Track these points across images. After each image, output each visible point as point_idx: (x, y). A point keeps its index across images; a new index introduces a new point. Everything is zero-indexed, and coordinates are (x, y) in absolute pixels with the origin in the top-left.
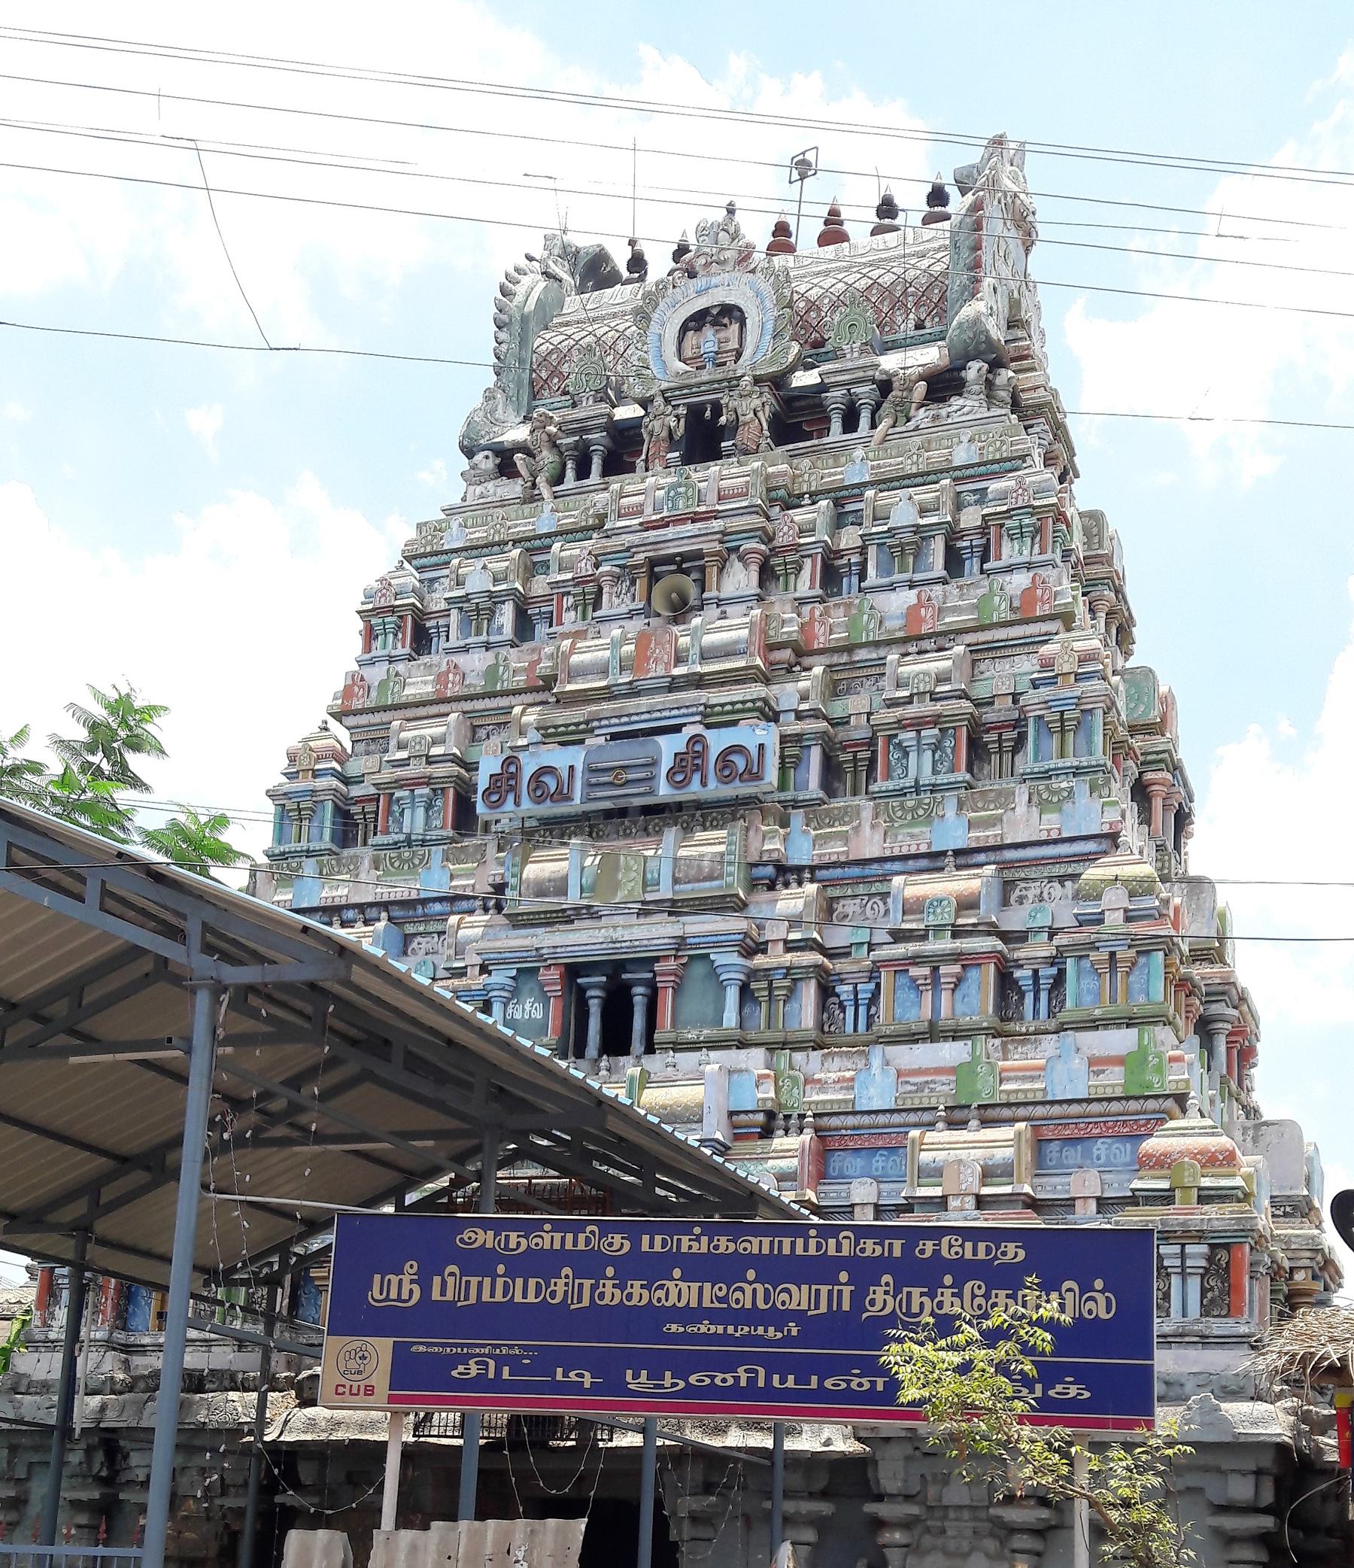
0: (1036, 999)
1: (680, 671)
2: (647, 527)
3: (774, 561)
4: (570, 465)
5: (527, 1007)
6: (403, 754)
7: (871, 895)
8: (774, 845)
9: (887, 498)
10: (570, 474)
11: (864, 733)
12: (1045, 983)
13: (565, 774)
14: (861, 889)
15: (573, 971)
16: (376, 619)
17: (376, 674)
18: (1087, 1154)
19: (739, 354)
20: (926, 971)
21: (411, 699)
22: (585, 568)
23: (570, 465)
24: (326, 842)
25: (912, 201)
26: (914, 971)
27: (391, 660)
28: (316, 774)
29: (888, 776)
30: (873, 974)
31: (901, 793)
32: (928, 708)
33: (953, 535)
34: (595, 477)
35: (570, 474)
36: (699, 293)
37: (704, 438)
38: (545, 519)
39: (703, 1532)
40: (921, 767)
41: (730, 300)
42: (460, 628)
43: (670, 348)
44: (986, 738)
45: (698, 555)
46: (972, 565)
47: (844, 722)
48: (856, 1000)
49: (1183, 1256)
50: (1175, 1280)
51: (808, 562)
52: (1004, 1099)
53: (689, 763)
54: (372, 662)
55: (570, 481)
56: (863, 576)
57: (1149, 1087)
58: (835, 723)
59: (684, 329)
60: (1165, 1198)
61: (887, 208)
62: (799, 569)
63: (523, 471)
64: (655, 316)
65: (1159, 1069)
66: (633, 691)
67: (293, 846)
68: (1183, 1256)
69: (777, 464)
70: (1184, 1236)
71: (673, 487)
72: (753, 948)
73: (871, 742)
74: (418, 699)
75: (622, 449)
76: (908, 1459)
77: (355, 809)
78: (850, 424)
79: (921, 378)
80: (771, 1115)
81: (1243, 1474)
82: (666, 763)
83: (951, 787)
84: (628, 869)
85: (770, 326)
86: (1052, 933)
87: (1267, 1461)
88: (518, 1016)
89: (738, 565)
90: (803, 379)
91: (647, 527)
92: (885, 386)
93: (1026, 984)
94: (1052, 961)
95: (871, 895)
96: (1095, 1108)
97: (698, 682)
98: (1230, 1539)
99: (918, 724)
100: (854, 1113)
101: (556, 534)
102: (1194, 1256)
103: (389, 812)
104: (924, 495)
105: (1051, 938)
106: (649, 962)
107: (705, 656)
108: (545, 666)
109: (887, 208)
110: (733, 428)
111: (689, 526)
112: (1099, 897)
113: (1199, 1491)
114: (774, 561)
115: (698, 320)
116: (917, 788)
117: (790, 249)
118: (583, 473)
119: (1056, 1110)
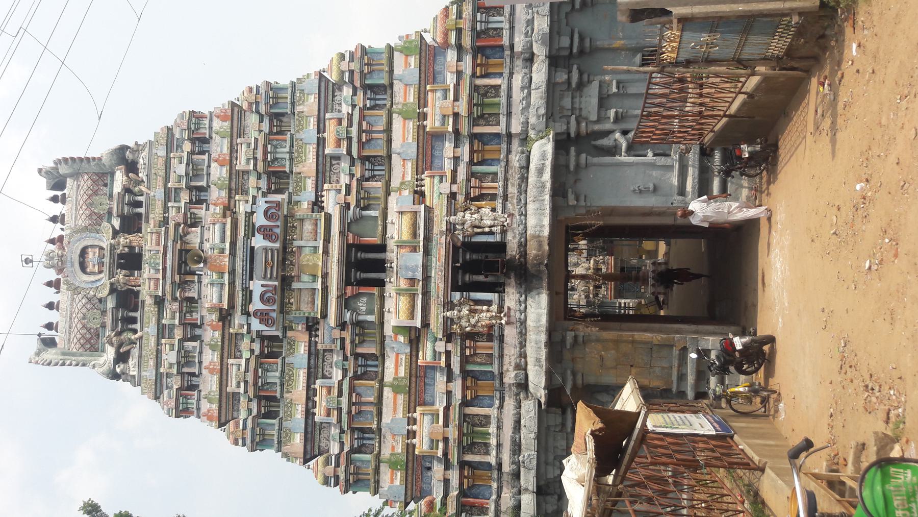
0: (379, 99)
2: (164, 278)
4: (130, 326)
6: (242, 385)
7: (331, 170)
8: (305, 205)
9: (173, 178)
10: (134, 326)
12: (361, 435)
13: (264, 289)
14: (328, 174)
15: (348, 283)
17: (205, 406)
18: (440, 73)
20: (364, 135)
21: (219, 359)
22: (176, 306)
23: (130, 326)
24: (275, 421)
25: (51, 295)
27: (199, 400)
29: (284, 166)
30: (357, 356)
31: (291, 159)
34: (137, 315)
35: (134, 326)
36: (72, 265)
37: (131, 261)
38: (151, 329)
39: (582, 198)
40: (274, 377)
41: (78, 252)
42: (190, 367)
43: (92, 278)
44: (266, 352)
45: (181, 251)
46: (198, 332)
48: (364, 366)
49: (475, 187)
50: (490, 26)
51: (192, 210)
52: (417, 100)
53: (267, 233)
56: (193, 375)
57: (406, 385)
60: (459, 31)
61: (50, 306)
62: (194, 214)
63: (129, 347)
64: (77, 284)
65: (411, 42)
66: (232, 272)
68: (475, 187)
69: (149, 227)
70: (474, 21)
71: (150, 265)
75: (127, 300)
76: (554, 121)
77: (263, 411)
78: (139, 204)
79: (128, 176)
80: (415, 192)
82: (262, 327)
84: (308, 260)
85: (93, 235)
88: (364, 309)
89: (188, 237)
90: (116, 223)
91: (164, 278)
92: (127, 190)
93: (373, 103)
94: (356, 359)
95: (331, 170)
96: (423, 68)
97: (233, 244)
99: (256, 376)
100: (407, 462)
101: (157, 369)
102: (481, 17)
104: (175, 162)
106: (349, 247)
107: (223, 240)
108: (214, 317)
109: (54, 219)
110: (131, 248)
113: (567, 14)
115: (83, 267)
117: (63, 216)
119: (420, 157)
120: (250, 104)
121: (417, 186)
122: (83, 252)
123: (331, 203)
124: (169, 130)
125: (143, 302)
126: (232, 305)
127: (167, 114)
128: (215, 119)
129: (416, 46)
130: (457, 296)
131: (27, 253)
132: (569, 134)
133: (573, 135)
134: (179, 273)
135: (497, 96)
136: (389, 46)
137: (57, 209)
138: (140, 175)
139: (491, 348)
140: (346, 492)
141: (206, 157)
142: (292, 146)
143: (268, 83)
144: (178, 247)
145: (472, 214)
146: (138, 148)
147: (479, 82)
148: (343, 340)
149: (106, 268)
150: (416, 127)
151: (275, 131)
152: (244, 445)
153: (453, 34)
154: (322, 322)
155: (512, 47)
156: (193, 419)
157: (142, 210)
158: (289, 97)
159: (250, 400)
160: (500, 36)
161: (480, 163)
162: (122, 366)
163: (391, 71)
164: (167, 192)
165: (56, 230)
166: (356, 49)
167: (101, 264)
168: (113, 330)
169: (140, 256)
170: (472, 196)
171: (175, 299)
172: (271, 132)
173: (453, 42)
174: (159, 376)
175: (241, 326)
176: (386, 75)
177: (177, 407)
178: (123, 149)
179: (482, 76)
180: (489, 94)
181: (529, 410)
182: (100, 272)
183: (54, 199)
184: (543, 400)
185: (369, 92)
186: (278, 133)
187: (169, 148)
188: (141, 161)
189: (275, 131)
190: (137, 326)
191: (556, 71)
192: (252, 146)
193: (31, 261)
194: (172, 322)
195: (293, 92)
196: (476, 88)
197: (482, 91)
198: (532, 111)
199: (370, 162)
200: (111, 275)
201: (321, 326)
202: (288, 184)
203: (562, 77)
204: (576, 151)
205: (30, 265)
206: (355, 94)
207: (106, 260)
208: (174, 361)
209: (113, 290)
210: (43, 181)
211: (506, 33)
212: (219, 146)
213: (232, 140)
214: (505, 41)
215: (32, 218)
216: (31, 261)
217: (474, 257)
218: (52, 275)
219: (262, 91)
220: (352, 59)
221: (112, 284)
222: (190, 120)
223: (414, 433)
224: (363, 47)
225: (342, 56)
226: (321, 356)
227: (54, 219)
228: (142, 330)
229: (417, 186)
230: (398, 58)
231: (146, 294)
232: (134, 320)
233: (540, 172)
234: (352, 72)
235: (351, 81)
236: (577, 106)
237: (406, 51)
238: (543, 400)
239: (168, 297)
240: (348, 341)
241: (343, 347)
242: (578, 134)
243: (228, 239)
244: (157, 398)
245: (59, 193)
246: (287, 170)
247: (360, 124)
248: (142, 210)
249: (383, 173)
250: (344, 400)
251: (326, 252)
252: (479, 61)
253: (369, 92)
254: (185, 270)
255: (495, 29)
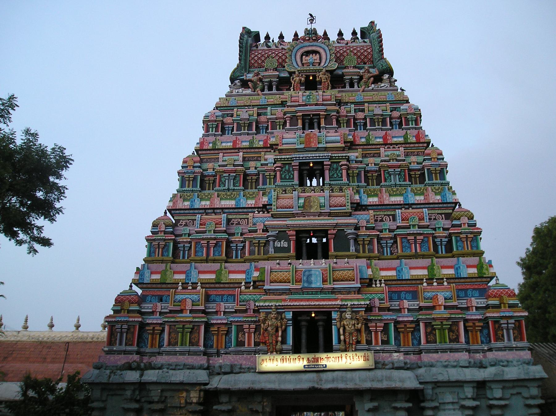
1: (320, 146)
3: (340, 119)
5: (282, 243)
9: (372, 107)
10: (266, 89)
11: (255, 172)
16: (207, 123)
17: (212, 139)
19: (320, 64)
20: (413, 237)
21: (224, 147)
26: (409, 238)
28: (194, 167)
31: (390, 186)
32: (395, 163)
33: (257, 123)
34: (274, 91)
35: (266, 89)
37: (311, 84)
38: (262, 99)
45: (319, 115)
47: (207, 170)
54: (208, 136)
55: (266, 91)
58: (204, 170)
59: (302, 55)
60: (498, 307)
67: (187, 188)
72: (357, 228)
73: (258, 174)
74: (226, 147)
78: (352, 86)
81: (534, 387)
83: (196, 191)
86: (189, 235)
87: (475, 385)
90: (340, 72)
91: (300, 106)
93: (439, 243)
98: (529, 406)
99: (229, 172)
102: (510, 323)
103: (220, 180)
104: (383, 106)
105: (189, 236)
109: (340, 34)
111: (314, 107)
112: (459, 219)
113: (520, 393)
114: (340, 119)
115: (307, 53)
116: (396, 185)
118: (270, 89)
120: (429, 155)
121: (380, 281)
122: (316, 52)
123: (363, 218)
124: (407, 102)
125: (283, 94)
126: (281, 151)
127: (416, 99)
128: (417, 131)
129: (485, 274)
130: (289, 315)
131: (317, 20)
132: (423, 401)
133: (422, 404)
134: (303, 115)
135: (451, 341)
136: (483, 253)
137: (348, 36)
138: (373, 85)
139: (249, 344)
140: (147, 240)
141: (389, 127)
142: (401, 185)
143: (446, 166)
144: (321, 113)
145: (354, 325)
146: (392, 82)
147: (462, 324)
148: (256, 231)
149: (306, 68)
150: (422, 277)
151: (411, 173)
152: (183, 167)
153: (497, 302)
154: (270, 215)
155: (490, 350)
156: (203, 132)
157: (348, 87)
158: (437, 182)
159: (256, 168)
160: (496, 340)
161: (396, 329)
162: (239, 84)
163: (463, 255)
164: (362, 103)
165: (333, 37)
166: (478, 229)
167: (308, 64)
168: (263, 76)
169: (315, 88)
170: (370, 325)
171: (285, 114)
172: (410, 170)
173: (490, 302)
174: (231, 108)
175: (266, 160)
176: (461, 251)
177: (209, 121)
178: (390, 72)
179: (465, 327)
180: (451, 334)
181: (202, 376)
182: (303, 64)
183: (354, 33)
184: (208, 387)
185: (447, 240)
186: (410, 175)
187: (391, 102)
188: (383, 85)
189: (411, 173)
190: (266, 91)
191: (473, 387)
192: (399, 158)
193: (311, 23)
194: (269, 114)
195: (442, 184)
196: (456, 324)
197: (454, 328)
198: (441, 370)
199: (393, 244)
200: (300, 72)
201: (266, 214)
202: (373, 185)
203: (469, 391)
204: (409, 408)
205: (309, 23)
206: (444, 229)
207: (312, 68)
208: (242, 117)
209: (291, 73)
210: (366, 25)
211: (499, 344)
212: (397, 135)
213: (402, 144)
214: (495, 344)
215: (339, 21)
216: (311, 23)
217: (321, 329)
218: (301, 34)
219: (440, 162)
220: (469, 225)
221: (294, 73)
222: (415, 114)
223: (186, 288)
224: (480, 233)
225: (471, 217)
226: (244, 216)
227: (340, 34)
228: (263, 95)
229: (380, 281)
230: (474, 260)
231: (287, 94)
232: (270, 89)
233: (389, 379)
234: (460, 226)
235: (453, 226)
236: (447, 407)
237: (480, 266)
238: (208, 387)
239: (286, 109)
240: (255, 235)
241: (250, 231)
242: (424, 409)
243: (329, 145)
244: (217, 108)
245: (359, 36)
246: (383, 183)
247: (421, 234)
248: (348, 87)
249: (386, 255)
250: (416, 230)
251: (320, 214)
252: (477, 324)
253: (447, 240)
254: (306, 119)
255: (503, 336)
